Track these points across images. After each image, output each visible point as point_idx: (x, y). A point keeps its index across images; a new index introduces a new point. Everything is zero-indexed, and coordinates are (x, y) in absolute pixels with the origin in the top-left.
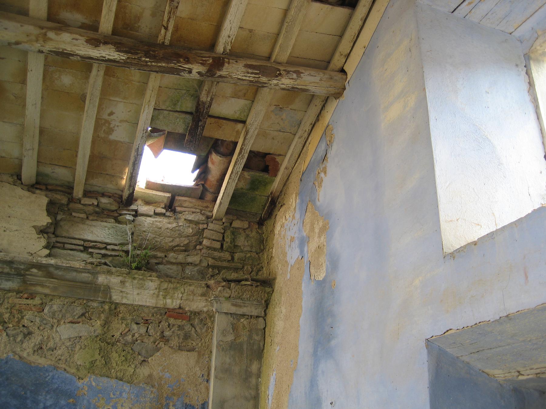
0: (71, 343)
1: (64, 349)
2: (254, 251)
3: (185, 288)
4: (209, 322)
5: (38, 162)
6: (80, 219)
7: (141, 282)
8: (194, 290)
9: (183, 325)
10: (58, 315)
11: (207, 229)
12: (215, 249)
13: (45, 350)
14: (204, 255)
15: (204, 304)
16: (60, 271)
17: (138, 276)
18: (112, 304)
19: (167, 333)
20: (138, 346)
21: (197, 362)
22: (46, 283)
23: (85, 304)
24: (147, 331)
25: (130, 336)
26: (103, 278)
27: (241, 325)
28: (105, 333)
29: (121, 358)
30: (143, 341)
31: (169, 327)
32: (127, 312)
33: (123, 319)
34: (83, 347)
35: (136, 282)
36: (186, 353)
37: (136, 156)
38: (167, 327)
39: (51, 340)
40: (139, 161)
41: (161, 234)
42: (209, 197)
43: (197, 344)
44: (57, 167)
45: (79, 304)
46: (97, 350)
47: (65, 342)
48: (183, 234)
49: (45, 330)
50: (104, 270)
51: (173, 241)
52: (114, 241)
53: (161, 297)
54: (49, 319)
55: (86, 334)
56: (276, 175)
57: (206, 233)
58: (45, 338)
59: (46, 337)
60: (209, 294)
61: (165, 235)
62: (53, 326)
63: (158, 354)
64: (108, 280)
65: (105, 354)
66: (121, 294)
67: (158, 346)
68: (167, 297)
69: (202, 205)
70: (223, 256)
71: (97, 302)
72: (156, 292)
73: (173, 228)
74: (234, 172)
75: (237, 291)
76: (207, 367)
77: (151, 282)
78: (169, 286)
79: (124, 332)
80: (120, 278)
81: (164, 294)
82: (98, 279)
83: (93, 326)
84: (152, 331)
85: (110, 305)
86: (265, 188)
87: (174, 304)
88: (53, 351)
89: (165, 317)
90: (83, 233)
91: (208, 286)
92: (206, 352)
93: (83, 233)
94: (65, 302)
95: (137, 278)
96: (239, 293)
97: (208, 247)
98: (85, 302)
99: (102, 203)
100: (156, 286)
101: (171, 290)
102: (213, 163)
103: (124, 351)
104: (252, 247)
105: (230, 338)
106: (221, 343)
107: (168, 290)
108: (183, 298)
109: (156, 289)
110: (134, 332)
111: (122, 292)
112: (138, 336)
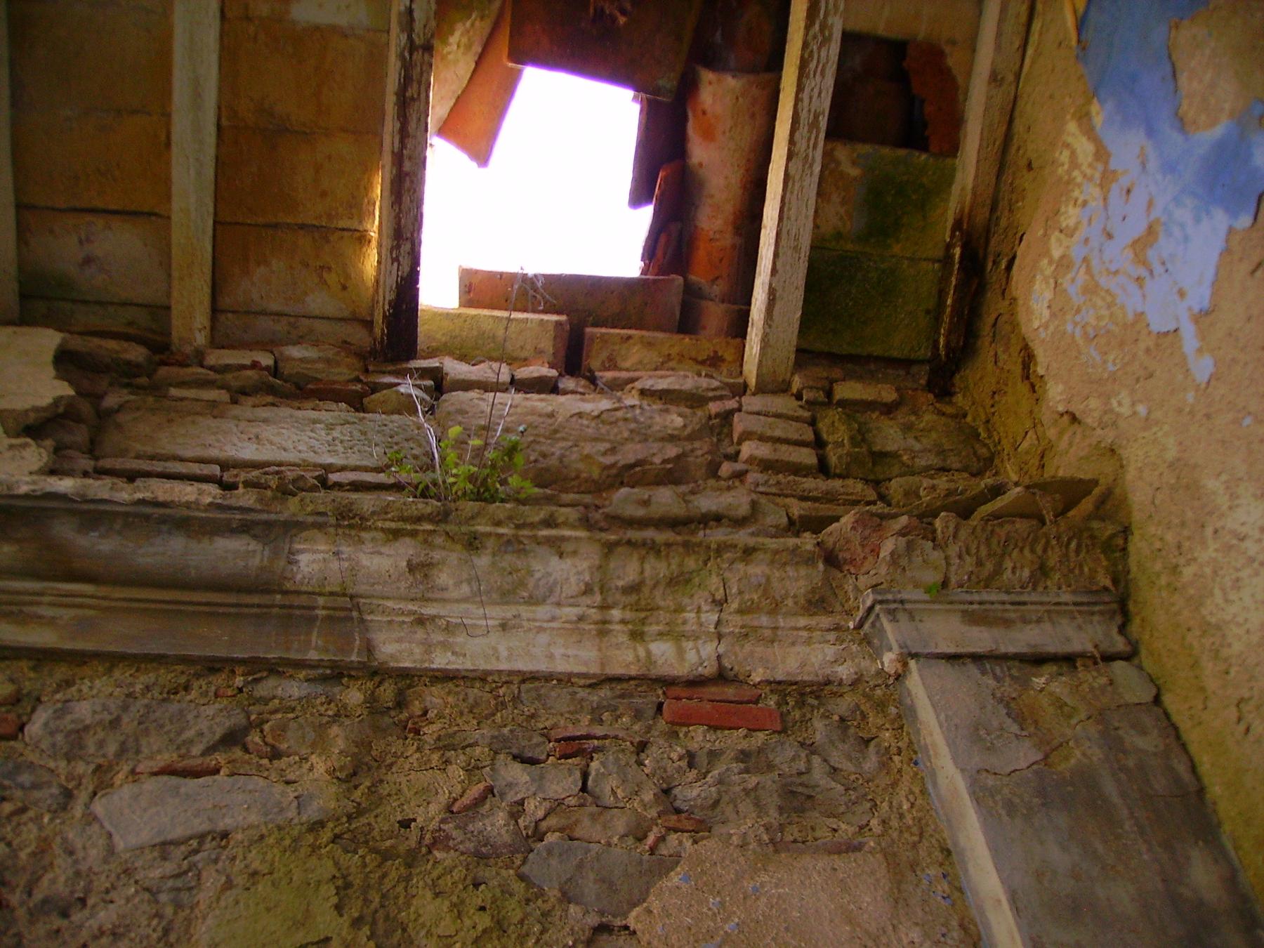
0: (169, 867)
1: (128, 900)
2: (956, 465)
3: (727, 575)
4: (880, 728)
5: (20, 207)
6: (203, 403)
7: (509, 560)
8: (768, 579)
9: (760, 751)
10: (101, 744)
11: (739, 410)
12: (797, 470)
13: (21, 912)
14: (761, 489)
15: (830, 651)
16: (102, 537)
17: (488, 529)
18: (380, 683)
19: (691, 793)
20: (554, 862)
21: (898, 899)
22: (39, 604)
23: (240, 690)
24: (584, 788)
25: (501, 818)
26: (320, 556)
27: (1044, 701)
28: (360, 811)
29: (468, 922)
30: (577, 834)
31: (691, 765)
32: (462, 714)
33: (446, 745)
34: (240, 880)
35: (483, 561)
36: (823, 862)
37: (407, 54)
38: (684, 764)
39: (58, 861)
40: (419, 83)
41: (556, 431)
42: (715, 314)
43: (861, 828)
44: (100, 222)
45: (211, 694)
46: (323, 888)
47: (138, 864)
48: (649, 432)
49: (25, 817)
50: (321, 509)
51: (613, 450)
52: (354, 460)
53: (620, 634)
54: (52, 764)
55: (253, 818)
56: (953, 148)
57: (740, 424)
58: (23, 855)
59: (28, 850)
60: (841, 594)
61: (574, 432)
62: (68, 795)
63: (675, 878)
64: (346, 564)
65: (373, 906)
66: (420, 634)
67: (664, 850)
68: (646, 629)
69: (693, 354)
70: (842, 490)
71: (302, 674)
72: (588, 607)
73: (602, 413)
74: (803, 115)
75: (968, 553)
76: (955, 923)
77: (556, 558)
78: (648, 573)
79: (466, 800)
80: (406, 550)
81: (628, 615)
82: (297, 562)
83: (288, 783)
84: (613, 782)
85: (370, 685)
86: (924, 217)
87: (691, 656)
88: (65, 914)
89: (662, 724)
90: (218, 441)
91: (831, 559)
92: (922, 853)
93: (218, 441)
94: (138, 687)
95: (489, 535)
96: (980, 563)
97: (767, 466)
98: (239, 681)
99: (294, 359)
100: (587, 578)
101: (658, 593)
102: (708, 135)
103: (476, 885)
104: (941, 452)
105: (1023, 755)
106: (991, 781)
107: (646, 590)
108: (725, 630)
109: (588, 591)
110: (519, 797)
111: (421, 621)
112: (540, 814)
